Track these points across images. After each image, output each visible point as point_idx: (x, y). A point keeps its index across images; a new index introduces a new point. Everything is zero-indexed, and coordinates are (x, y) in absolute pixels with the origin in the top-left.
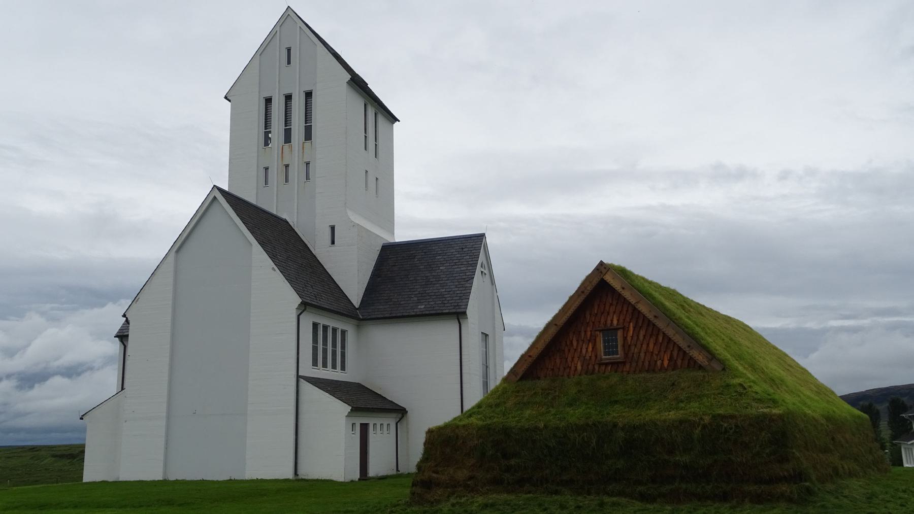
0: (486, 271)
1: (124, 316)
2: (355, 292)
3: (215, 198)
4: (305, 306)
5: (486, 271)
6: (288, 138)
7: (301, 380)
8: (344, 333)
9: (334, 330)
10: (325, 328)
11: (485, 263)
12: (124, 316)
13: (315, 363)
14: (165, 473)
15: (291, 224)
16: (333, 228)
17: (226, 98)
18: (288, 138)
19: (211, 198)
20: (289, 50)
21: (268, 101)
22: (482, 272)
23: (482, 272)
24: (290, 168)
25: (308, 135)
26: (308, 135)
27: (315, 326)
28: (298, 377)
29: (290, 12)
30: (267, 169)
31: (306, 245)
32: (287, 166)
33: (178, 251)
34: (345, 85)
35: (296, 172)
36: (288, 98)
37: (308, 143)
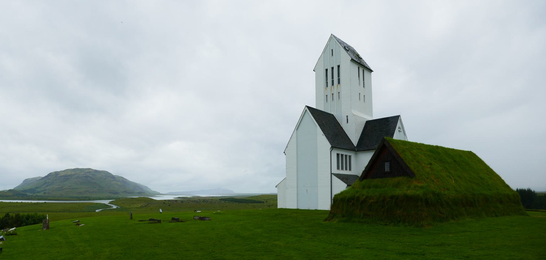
0: (402, 130)
1: (284, 153)
2: (355, 141)
3: (306, 110)
4: (333, 148)
5: (402, 130)
6: (333, 84)
7: (332, 175)
8: (350, 157)
9: (346, 156)
10: (346, 156)
11: (401, 126)
12: (284, 153)
13: (338, 168)
14: (297, 206)
15: (335, 116)
16: (347, 116)
17: (314, 71)
18: (333, 84)
19: (305, 110)
20: (332, 50)
21: (327, 70)
22: (399, 131)
23: (399, 131)
24: (334, 95)
25: (339, 83)
26: (339, 83)
27: (338, 155)
28: (331, 174)
29: (332, 36)
30: (327, 96)
31: (339, 123)
32: (333, 94)
33: (297, 130)
34: (350, 61)
35: (336, 96)
36: (333, 68)
37: (339, 85)
